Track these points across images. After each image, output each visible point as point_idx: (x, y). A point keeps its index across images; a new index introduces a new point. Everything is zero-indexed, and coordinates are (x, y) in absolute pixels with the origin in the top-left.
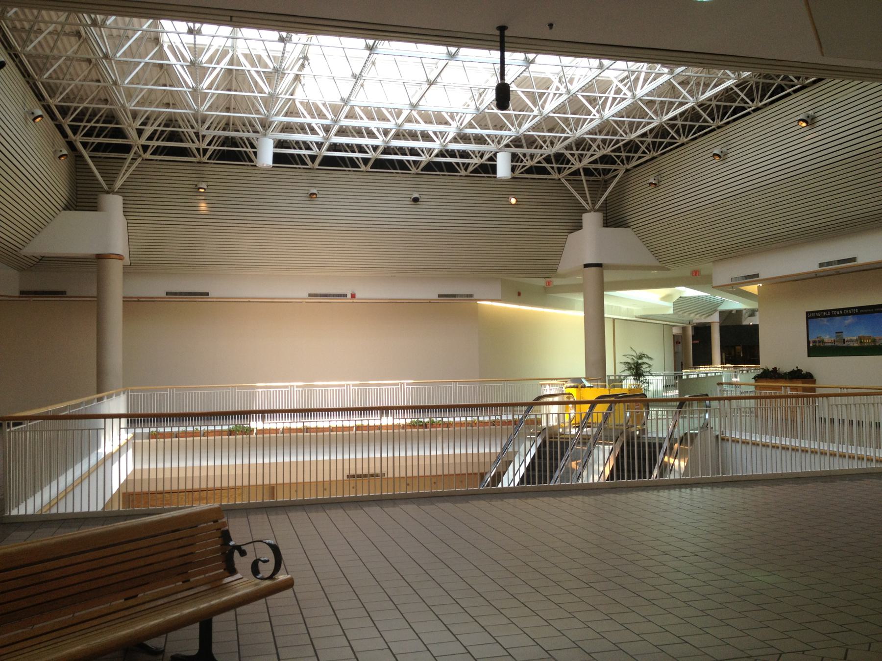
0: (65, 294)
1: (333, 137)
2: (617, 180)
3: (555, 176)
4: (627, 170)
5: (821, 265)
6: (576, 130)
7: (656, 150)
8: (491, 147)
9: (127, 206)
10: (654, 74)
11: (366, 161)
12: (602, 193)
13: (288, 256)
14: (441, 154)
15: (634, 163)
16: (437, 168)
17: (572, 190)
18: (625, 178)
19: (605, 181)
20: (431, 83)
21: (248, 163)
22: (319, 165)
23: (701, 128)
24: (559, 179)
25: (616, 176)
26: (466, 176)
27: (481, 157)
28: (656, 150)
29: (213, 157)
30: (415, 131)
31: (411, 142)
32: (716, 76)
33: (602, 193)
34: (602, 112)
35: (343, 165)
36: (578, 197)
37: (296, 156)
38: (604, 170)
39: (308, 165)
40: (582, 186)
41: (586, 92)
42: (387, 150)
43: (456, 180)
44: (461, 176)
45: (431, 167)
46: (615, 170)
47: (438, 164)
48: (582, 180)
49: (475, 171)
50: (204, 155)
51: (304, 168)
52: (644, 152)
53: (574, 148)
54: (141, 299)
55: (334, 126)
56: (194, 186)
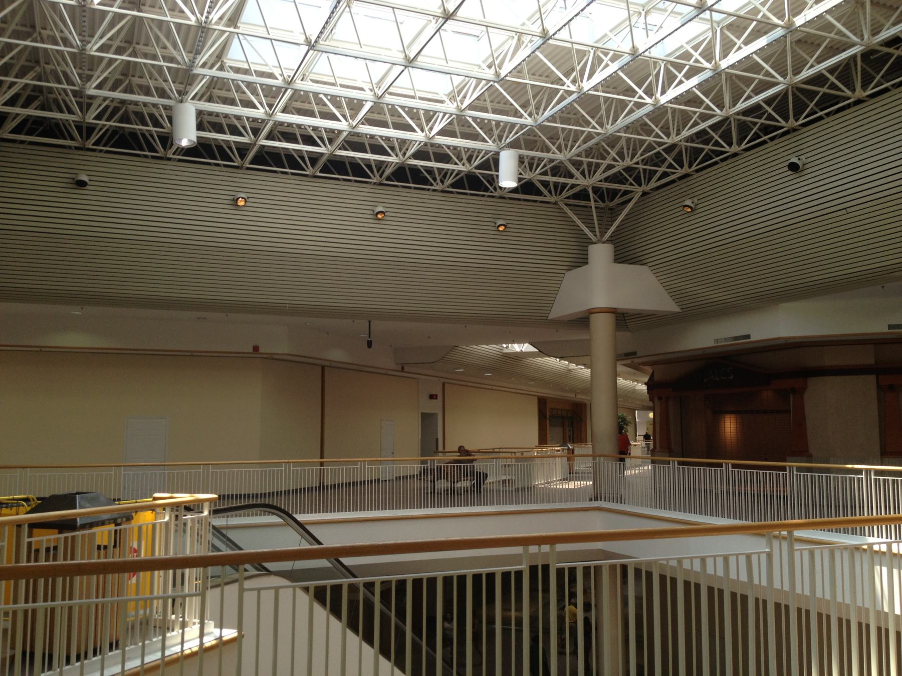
0: (750, 338)
1: (278, 114)
2: (631, 205)
3: (553, 199)
4: (644, 194)
5: (890, 327)
6: (538, 114)
7: (568, 149)
8: (490, 145)
9: (584, 252)
10: (755, 23)
11: (314, 159)
12: (607, 227)
13: (438, 303)
14: (420, 154)
15: (653, 184)
16: (336, 170)
17: (579, 222)
18: (642, 203)
19: (611, 209)
20: (448, 16)
21: (147, 153)
22: (251, 163)
23: (766, 130)
24: (556, 203)
25: (630, 200)
26: (443, 191)
27: (469, 159)
28: (568, 149)
29: (104, 142)
30: (417, 109)
31: (368, 127)
32: (754, 17)
33: (607, 227)
34: (580, 83)
35: (273, 164)
36: (587, 231)
37: (305, 153)
38: (556, 185)
39: (157, 152)
40: (590, 217)
41: (814, 85)
42: (355, 143)
43: (367, 189)
44: (434, 190)
45: (404, 174)
46: (626, 193)
47: (415, 170)
48: (591, 207)
49: (458, 184)
50: (88, 138)
51: (225, 166)
52: (670, 166)
53: (583, 155)
54: (194, 354)
55: (286, 90)
56: (371, 212)
